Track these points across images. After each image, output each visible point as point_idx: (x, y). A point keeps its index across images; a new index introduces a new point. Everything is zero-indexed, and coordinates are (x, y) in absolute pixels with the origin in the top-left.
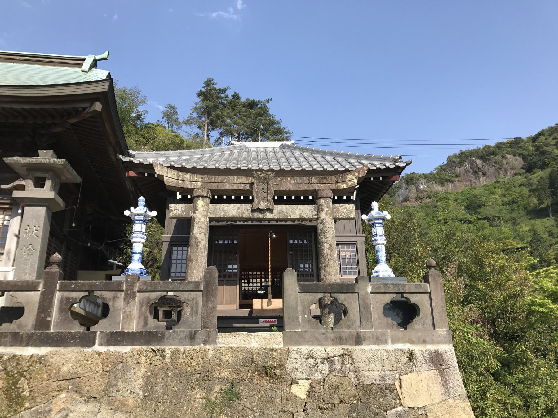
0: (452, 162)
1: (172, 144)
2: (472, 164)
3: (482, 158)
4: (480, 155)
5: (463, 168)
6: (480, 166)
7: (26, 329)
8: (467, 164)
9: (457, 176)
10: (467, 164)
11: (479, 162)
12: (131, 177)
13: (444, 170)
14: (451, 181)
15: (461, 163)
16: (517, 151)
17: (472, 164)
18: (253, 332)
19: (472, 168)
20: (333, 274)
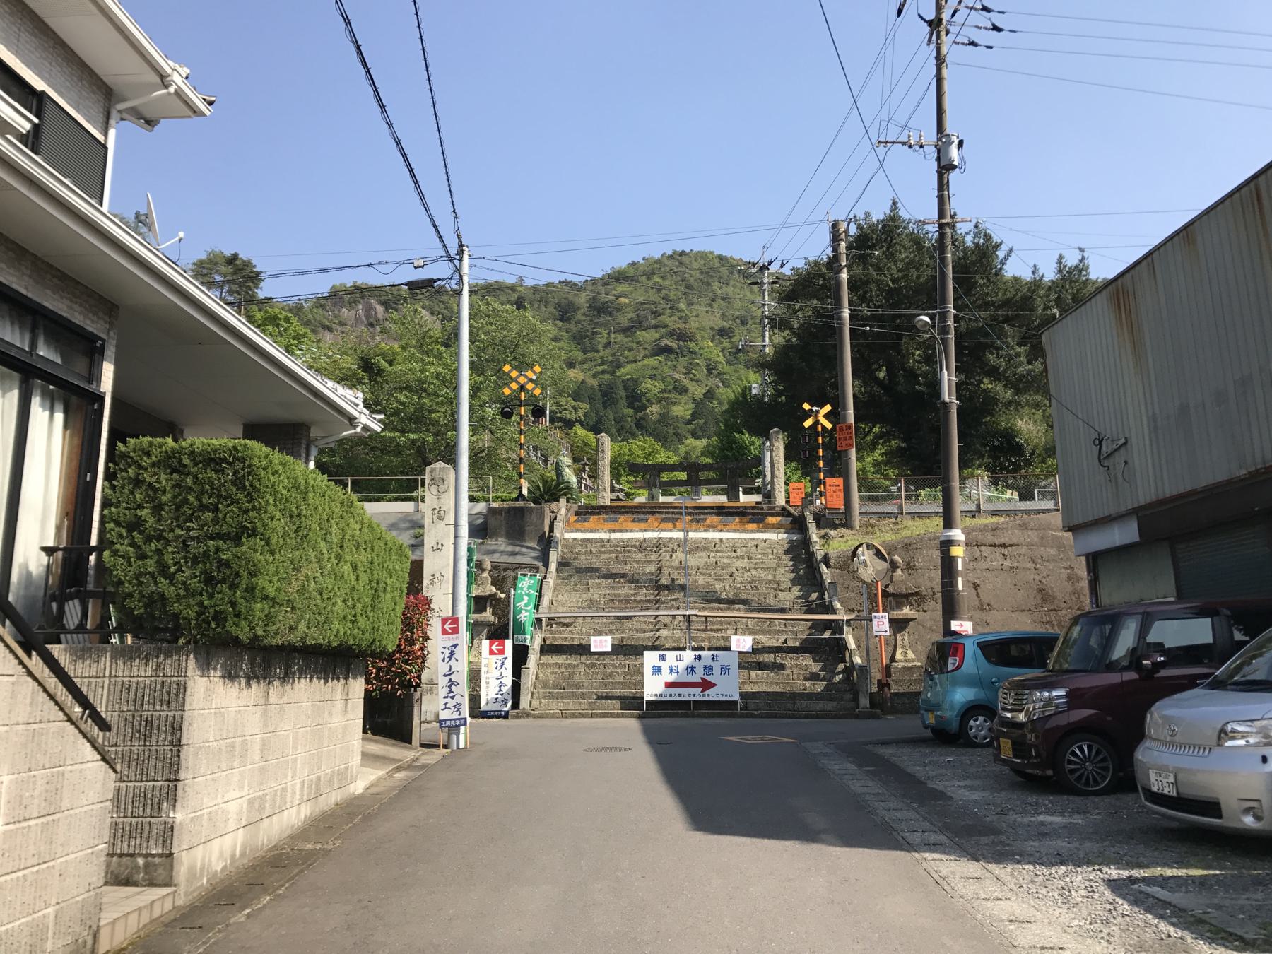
0: (337, 297)
1: (1212, 885)
2: (368, 309)
3: (386, 304)
4: (383, 299)
5: (353, 313)
6: (380, 316)
7: (259, 291)
8: (360, 307)
9: (342, 324)
10: (360, 307)
11: (380, 309)
12: (137, 863)
13: (322, 306)
14: (330, 330)
15: (352, 304)
16: (437, 308)
17: (368, 309)
18: (1106, 517)
19: (367, 317)
20: (580, 431)
